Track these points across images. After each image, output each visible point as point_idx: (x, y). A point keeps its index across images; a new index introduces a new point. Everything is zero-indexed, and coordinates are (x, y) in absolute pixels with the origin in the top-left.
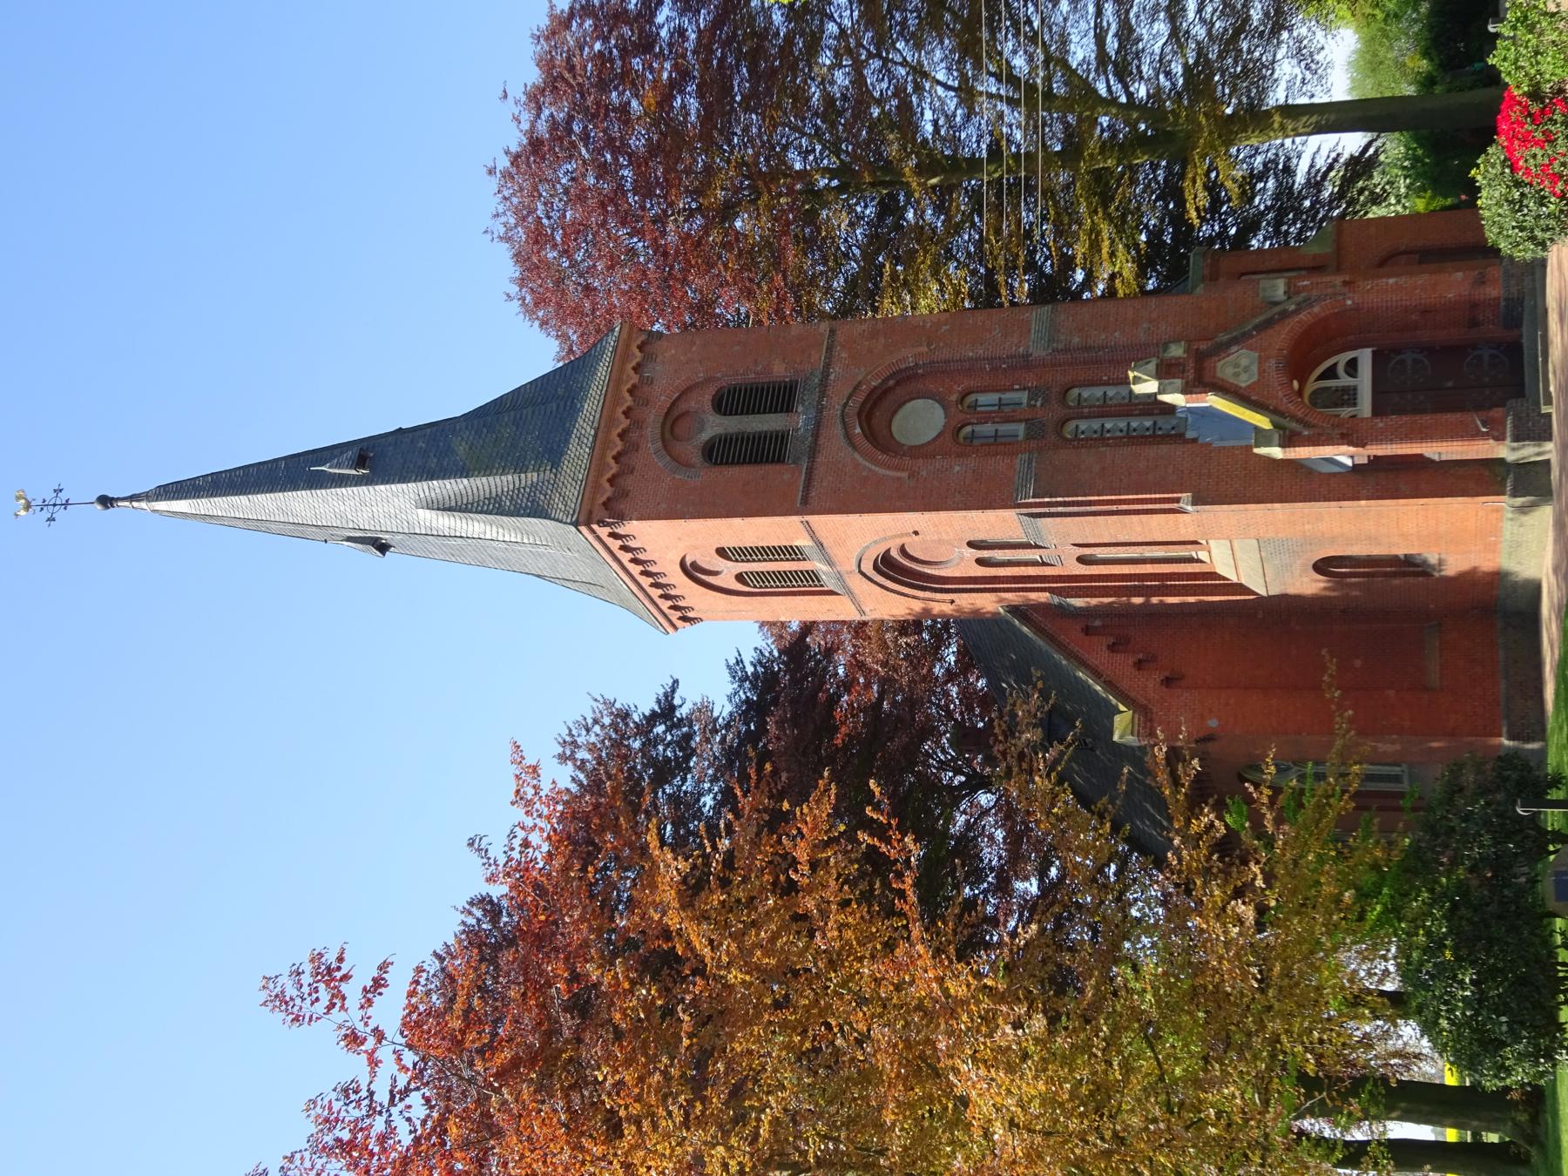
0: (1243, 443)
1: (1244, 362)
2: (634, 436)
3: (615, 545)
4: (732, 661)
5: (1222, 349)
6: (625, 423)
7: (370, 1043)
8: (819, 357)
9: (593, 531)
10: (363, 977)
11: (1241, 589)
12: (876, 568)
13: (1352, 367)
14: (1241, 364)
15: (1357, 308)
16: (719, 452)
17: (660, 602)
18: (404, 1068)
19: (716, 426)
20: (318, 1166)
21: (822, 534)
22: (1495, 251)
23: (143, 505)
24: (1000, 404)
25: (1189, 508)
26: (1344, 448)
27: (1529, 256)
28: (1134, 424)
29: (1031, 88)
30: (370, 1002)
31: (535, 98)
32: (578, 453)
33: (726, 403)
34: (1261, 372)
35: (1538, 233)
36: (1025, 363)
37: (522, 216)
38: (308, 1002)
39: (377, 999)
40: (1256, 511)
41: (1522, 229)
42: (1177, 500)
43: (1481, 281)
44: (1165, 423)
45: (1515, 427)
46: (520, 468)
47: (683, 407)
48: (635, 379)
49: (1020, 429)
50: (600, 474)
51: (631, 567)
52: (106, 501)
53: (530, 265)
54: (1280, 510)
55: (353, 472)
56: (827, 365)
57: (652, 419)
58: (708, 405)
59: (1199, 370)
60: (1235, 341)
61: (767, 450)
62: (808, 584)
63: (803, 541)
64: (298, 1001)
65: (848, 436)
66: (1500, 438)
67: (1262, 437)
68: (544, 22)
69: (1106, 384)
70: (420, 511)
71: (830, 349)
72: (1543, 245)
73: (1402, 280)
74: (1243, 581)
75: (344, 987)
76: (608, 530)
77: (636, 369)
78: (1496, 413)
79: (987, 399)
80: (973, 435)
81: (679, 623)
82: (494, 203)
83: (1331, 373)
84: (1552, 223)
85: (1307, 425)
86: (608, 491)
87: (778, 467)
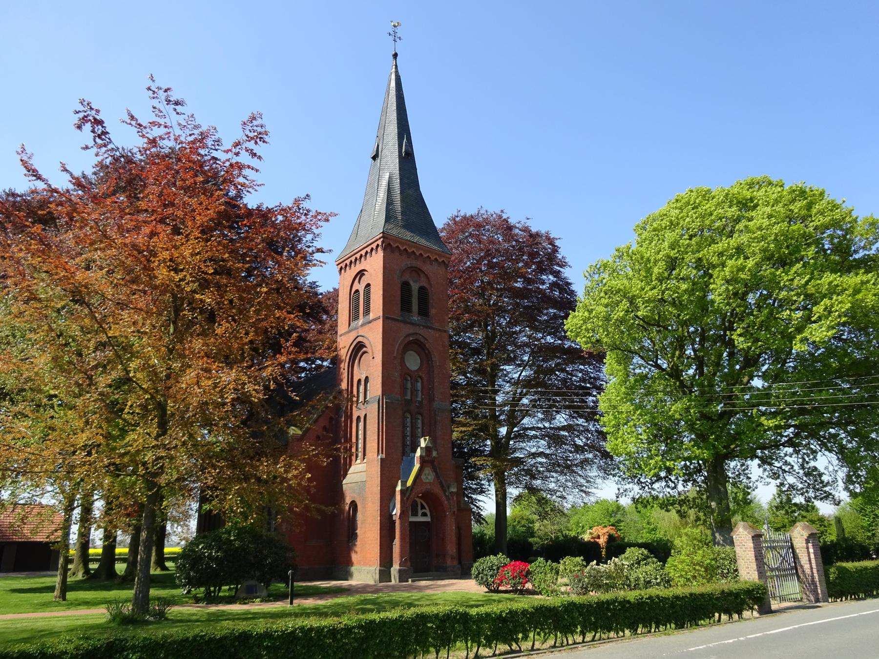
0: (401, 476)
1: (430, 477)
2: (413, 256)
3: (374, 246)
4: (317, 284)
5: (434, 469)
6: (418, 254)
7: (234, 150)
8: (437, 326)
9: (380, 238)
10: (257, 149)
11: (345, 474)
12: (360, 342)
13: (424, 515)
14: (429, 476)
15: (445, 516)
16: (405, 287)
17: (349, 260)
18: (224, 163)
19: (415, 287)
20: (188, 126)
21: (374, 323)
22: (475, 561)
23: (394, 70)
24: (417, 390)
25: (379, 457)
26: (399, 512)
27: (473, 572)
28: (408, 438)
29: (517, 405)
30: (247, 151)
31: (526, 230)
32: (408, 235)
33: (422, 290)
34: (426, 483)
35: (481, 575)
36: (431, 399)
37: (487, 221)
38: (251, 128)
39: (248, 154)
40: (377, 480)
41: (483, 570)
42: (382, 453)
43: (452, 558)
44: (408, 449)
45: (404, 570)
46: (403, 213)
47: (422, 275)
48: (433, 258)
49: (408, 397)
50: (400, 243)
51: (364, 251)
52: (395, 56)
53: (467, 221)
54: (377, 489)
55: (403, 150)
56: (434, 329)
57: (418, 264)
58: (422, 284)
59: (427, 462)
60: (437, 474)
61: (405, 305)
62: (354, 315)
63: (372, 316)
64: (251, 125)
65: (409, 335)
66: (400, 565)
67: (404, 483)
68: (552, 236)
69: (423, 429)
70: (388, 174)
71: (440, 330)
72: (477, 577)
73: (454, 531)
74: (348, 476)
75: (253, 142)
76: (380, 244)
77: (436, 259)
78: (409, 564)
79: (419, 385)
80: (407, 380)
81: (340, 266)
82: (491, 211)
83: (423, 507)
84: (485, 579)
85: (408, 499)
86: (395, 245)
87: (400, 308)
